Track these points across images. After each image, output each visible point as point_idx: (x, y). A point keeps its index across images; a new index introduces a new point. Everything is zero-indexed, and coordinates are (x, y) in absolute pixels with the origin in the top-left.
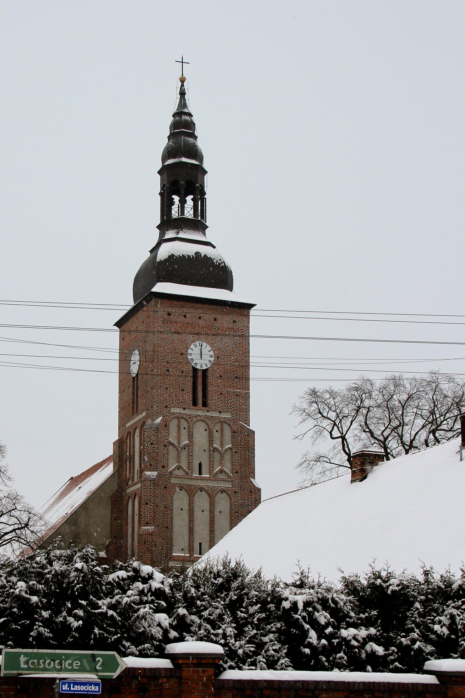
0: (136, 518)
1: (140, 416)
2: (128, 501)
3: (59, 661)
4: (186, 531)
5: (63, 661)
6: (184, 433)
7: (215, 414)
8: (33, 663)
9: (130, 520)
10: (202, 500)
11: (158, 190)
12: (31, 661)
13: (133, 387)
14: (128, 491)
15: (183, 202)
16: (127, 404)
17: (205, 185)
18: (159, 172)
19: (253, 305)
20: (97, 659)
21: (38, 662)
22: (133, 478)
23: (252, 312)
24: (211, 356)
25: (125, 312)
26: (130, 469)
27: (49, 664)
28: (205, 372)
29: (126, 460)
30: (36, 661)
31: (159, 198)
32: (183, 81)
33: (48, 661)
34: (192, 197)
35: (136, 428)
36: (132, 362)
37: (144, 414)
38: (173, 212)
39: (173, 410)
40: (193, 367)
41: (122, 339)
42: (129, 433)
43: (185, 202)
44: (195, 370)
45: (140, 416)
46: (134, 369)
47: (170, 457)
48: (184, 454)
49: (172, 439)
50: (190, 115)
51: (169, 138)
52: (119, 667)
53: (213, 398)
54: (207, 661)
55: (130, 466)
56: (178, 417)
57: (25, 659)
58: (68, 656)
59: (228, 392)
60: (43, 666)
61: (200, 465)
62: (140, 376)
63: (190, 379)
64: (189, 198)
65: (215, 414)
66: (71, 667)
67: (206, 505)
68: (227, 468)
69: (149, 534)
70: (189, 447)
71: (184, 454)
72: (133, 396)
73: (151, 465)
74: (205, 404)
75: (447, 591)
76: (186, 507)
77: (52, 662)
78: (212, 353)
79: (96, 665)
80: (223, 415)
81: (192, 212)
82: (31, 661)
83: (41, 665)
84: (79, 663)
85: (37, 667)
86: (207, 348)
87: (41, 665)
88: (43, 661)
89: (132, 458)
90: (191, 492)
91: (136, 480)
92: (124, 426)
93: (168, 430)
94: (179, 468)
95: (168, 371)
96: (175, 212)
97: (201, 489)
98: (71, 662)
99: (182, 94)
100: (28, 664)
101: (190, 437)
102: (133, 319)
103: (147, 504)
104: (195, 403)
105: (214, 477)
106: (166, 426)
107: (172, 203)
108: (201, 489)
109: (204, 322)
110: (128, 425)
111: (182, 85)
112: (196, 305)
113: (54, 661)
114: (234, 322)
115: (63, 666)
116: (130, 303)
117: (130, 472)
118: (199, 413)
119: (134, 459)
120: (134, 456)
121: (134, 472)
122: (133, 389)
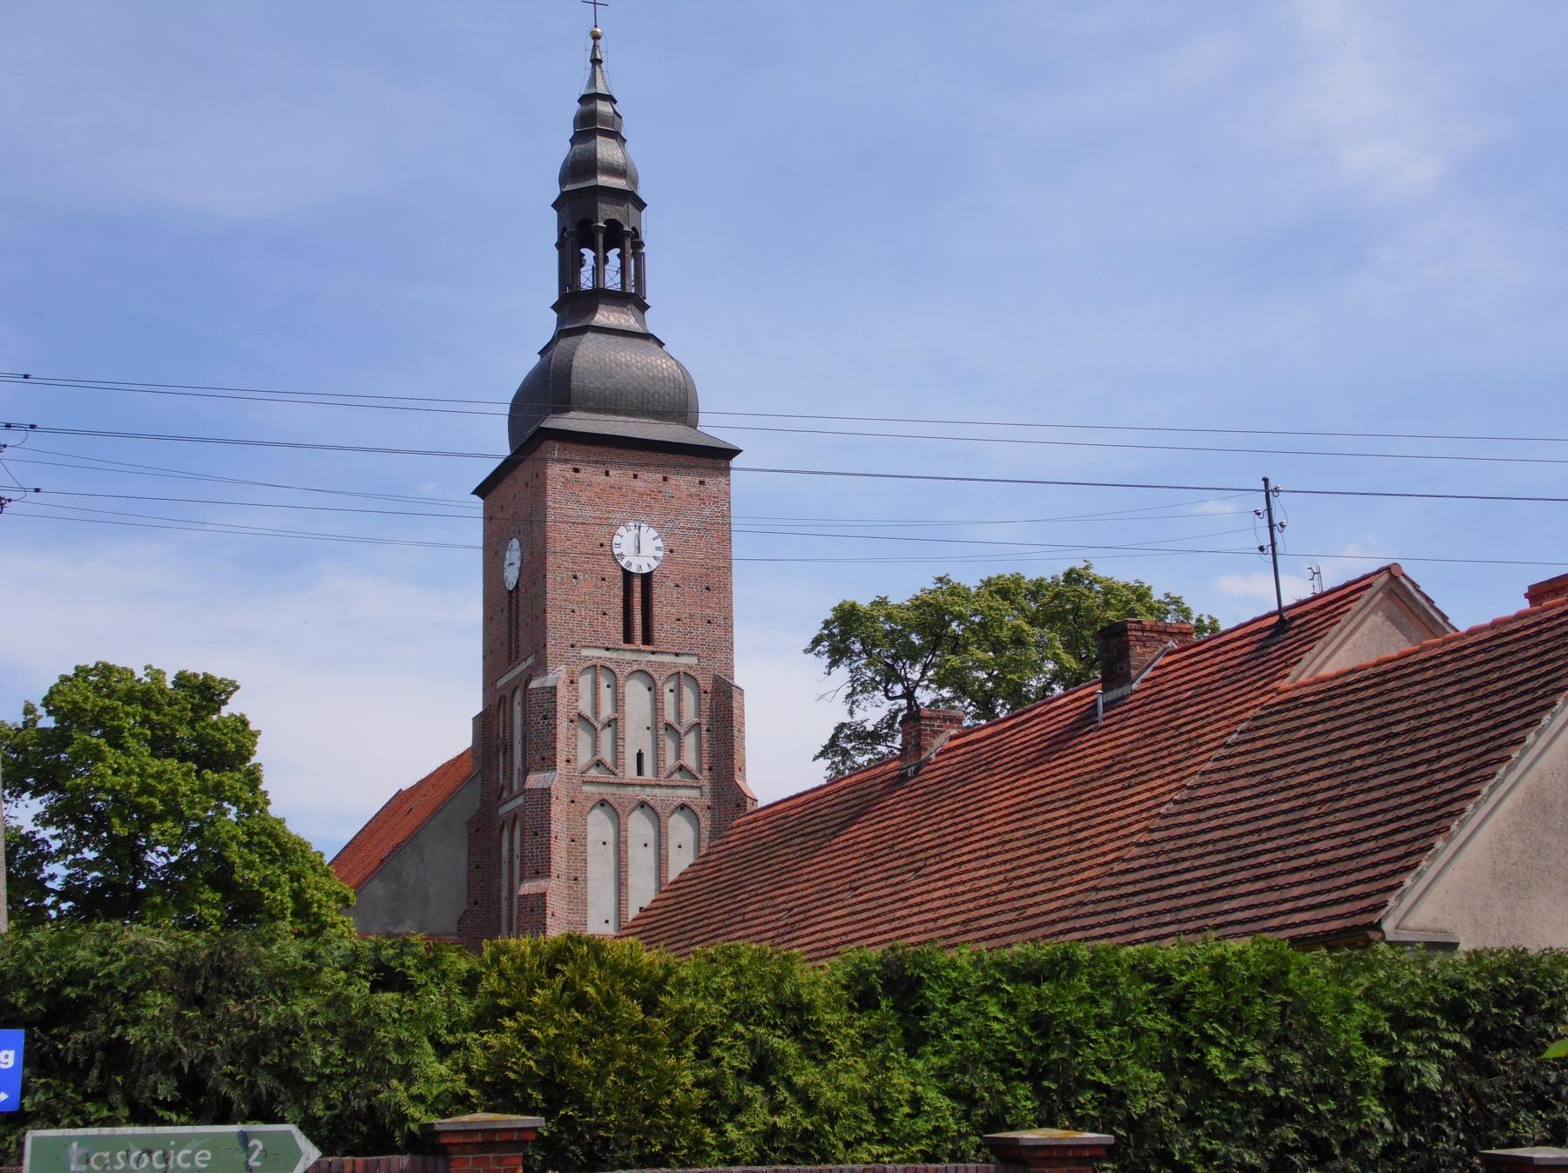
0: (517, 862)
1: (524, 666)
2: (502, 830)
3: (161, 1152)
4: (611, 885)
5: (172, 1152)
6: (606, 695)
8: (100, 1160)
9: (505, 868)
12: (96, 1155)
13: (511, 609)
14: (502, 811)
15: (600, 262)
16: (499, 643)
17: (643, 229)
18: (555, 205)
19: (736, 452)
20: (251, 1144)
21: (113, 1157)
22: (511, 786)
23: (735, 462)
24: (658, 549)
25: (495, 464)
26: (504, 768)
27: (138, 1160)
28: (647, 578)
29: (498, 750)
30: (107, 1154)
33: (135, 1154)
34: (617, 251)
35: (517, 687)
36: (507, 563)
37: (530, 661)
38: (583, 279)
40: (624, 570)
41: (489, 519)
42: (502, 698)
43: (606, 260)
44: (627, 576)
45: (524, 666)
46: (511, 576)
47: (580, 744)
48: (606, 736)
52: (302, 1160)
54: (505, 1137)
55: (504, 763)
56: (595, 666)
57: (83, 1150)
58: (182, 1141)
59: (691, 616)
60: (122, 1165)
61: (640, 756)
62: (522, 589)
63: (618, 591)
64: (613, 254)
66: (188, 1165)
67: (609, 832)
68: (690, 760)
71: (606, 736)
72: (510, 627)
73: (543, 759)
74: (647, 639)
77: (145, 1155)
78: (659, 543)
79: (248, 1156)
81: (618, 279)
82: (96, 1155)
83: (118, 1164)
84: (209, 1154)
85: (108, 1168)
87: (118, 1164)
88: (124, 1153)
89: (508, 749)
92: (493, 684)
93: (576, 689)
95: (575, 577)
96: (586, 280)
98: (189, 1152)
100: (88, 1161)
101: (618, 702)
102: (509, 481)
103: (536, 834)
104: (628, 637)
106: (572, 682)
107: (580, 262)
108: (643, 804)
109: (643, 484)
112: (626, 453)
113: (150, 1153)
114: (702, 483)
115: (171, 1163)
116: (503, 448)
117: (504, 775)
119: (512, 748)
120: (512, 742)
121: (512, 774)
122: (510, 615)
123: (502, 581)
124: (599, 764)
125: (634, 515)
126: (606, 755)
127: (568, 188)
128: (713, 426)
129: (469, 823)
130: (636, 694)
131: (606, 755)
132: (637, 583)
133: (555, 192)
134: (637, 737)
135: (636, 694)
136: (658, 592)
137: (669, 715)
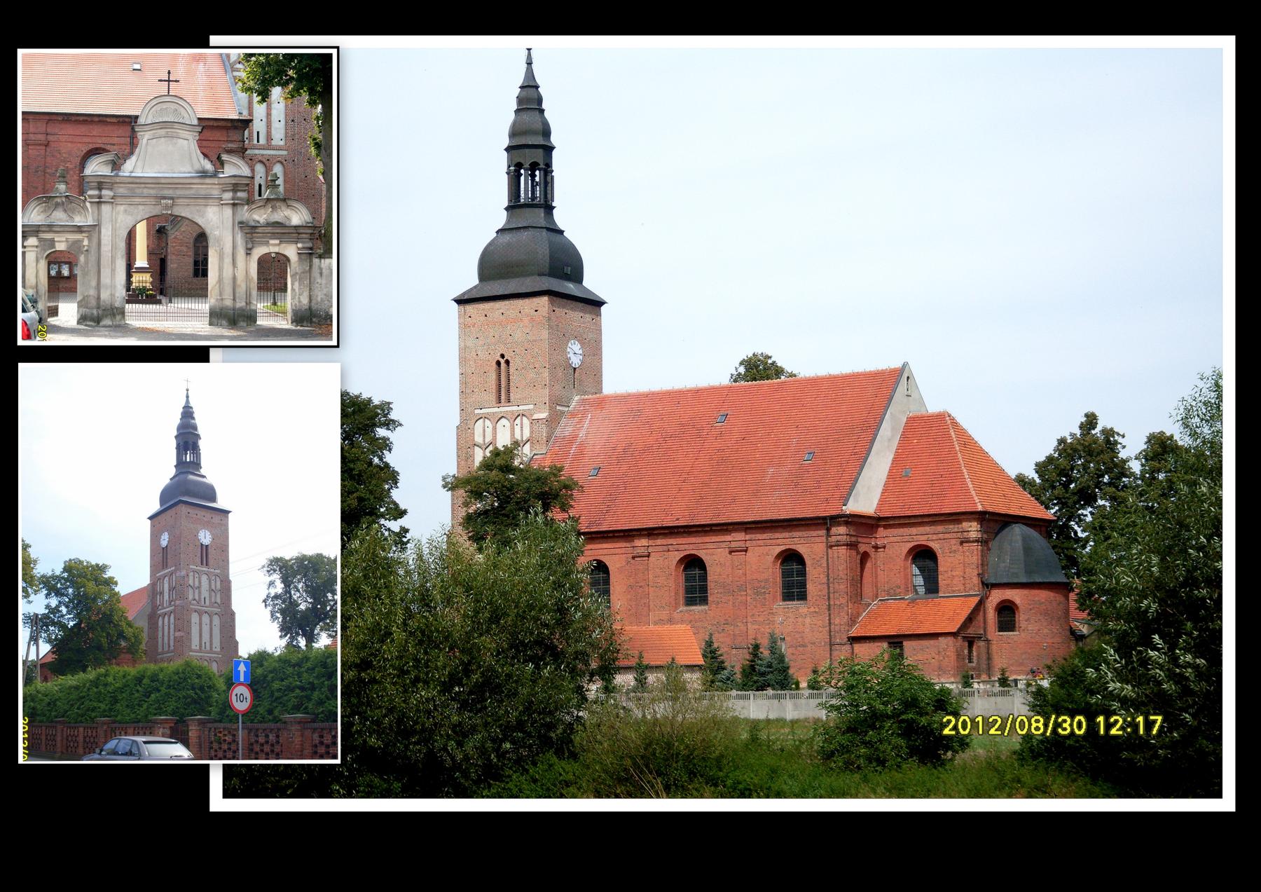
4: (198, 635)
6: (197, 580)
7: (212, 570)
9: (160, 629)
10: (206, 619)
11: (175, 446)
14: (159, 612)
23: (230, 514)
28: (207, 546)
31: (175, 451)
32: (187, 390)
39: (191, 567)
44: (202, 544)
48: (197, 591)
49: (191, 582)
50: (191, 408)
51: (181, 419)
53: (211, 562)
61: (205, 598)
63: (200, 547)
65: (212, 570)
68: (219, 600)
69: (1191, 468)
70: (199, 587)
71: (197, 591)
75: (1132, 658)
76: (198, 622)
80: (216, 571)
86: (208, 533)
90: (200, 614)
91: (165, 605)
92: (155, 575)
94: (194, 600)
97: (206, 612)
99: (187, 397)
101: (200, 582)
105: (212, 605)
108: (206, 612)
110: (158, 575)
111: (187, 393)
118: (204, 569)
123: (159, 545)
124: (194, 600)
125: (204, 528)
126: (197, 598)
127: (181, 431)
128: (221, 503)
129: (148, 615)
130: (204, 578)
131: (197, 598)
132: (204, 547)
133: (506, 142)
134: (205, 594)
135: (204, 578)
136: (210, 550)
137: (213, 587)
